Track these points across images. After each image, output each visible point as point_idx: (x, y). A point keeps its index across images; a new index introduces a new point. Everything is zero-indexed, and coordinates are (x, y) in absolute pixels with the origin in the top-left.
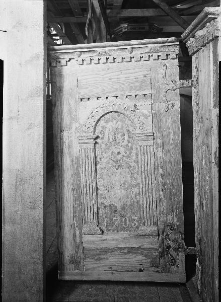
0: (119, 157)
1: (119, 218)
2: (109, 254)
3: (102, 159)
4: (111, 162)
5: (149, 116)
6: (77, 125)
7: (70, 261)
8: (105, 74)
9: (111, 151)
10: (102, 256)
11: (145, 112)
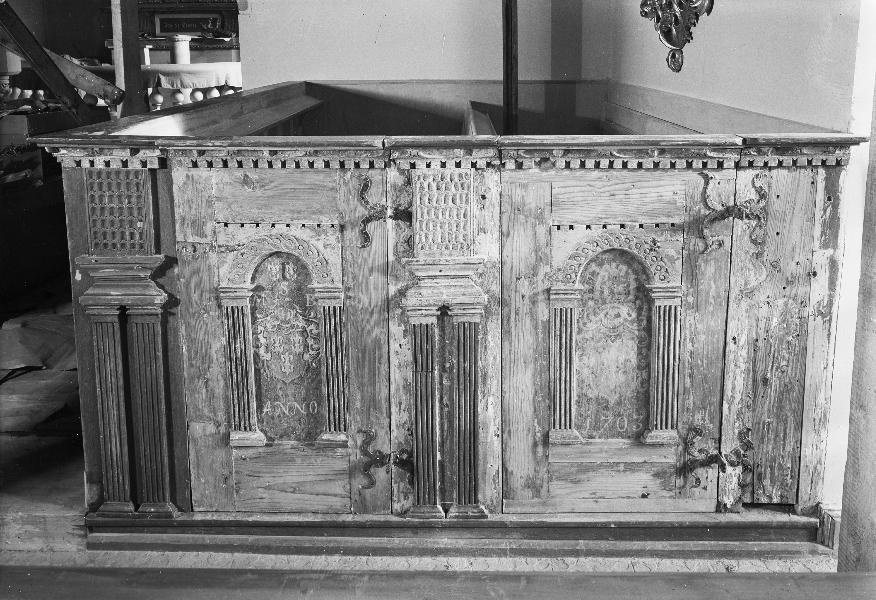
0: (617, 322)
1: (611, 418)
2: (591, 474)
3: (588, 325)
4: (603, 330)
5: (678, 258)
6: (547, 269)
7: (525, 486)
8: (604, 186)
9: (605, 312)
10: (583, 477)
11: (672, 252)
